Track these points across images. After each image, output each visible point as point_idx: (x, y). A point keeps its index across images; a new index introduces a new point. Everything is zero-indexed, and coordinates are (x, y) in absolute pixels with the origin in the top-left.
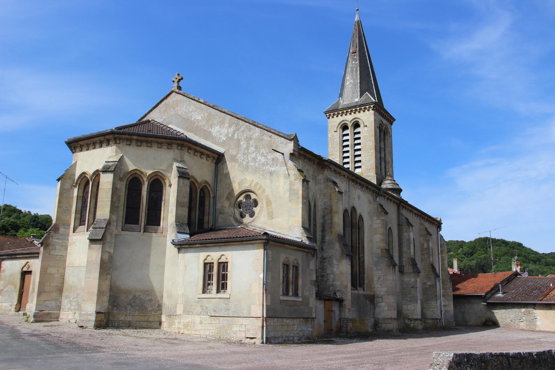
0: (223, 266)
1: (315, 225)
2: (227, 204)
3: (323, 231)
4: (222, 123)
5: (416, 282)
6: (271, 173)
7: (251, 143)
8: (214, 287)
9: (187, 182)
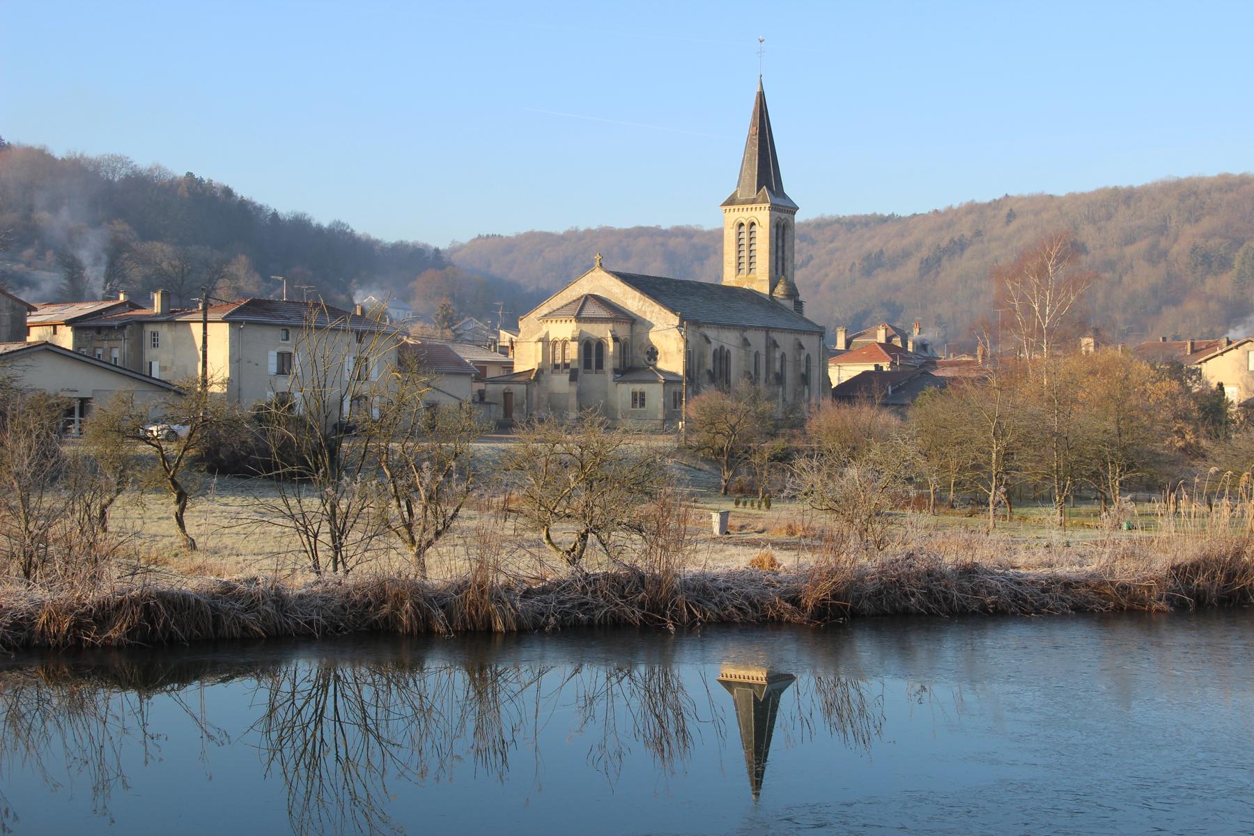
0: (643, 394)
1: (693, 364)
2: (639, 352)
3: (699, 367)
4: (634, 298)
5: (778, 391)
6: (666, 336)
7: (654, 314)
8: (638, 404)
9: (618, 344)
